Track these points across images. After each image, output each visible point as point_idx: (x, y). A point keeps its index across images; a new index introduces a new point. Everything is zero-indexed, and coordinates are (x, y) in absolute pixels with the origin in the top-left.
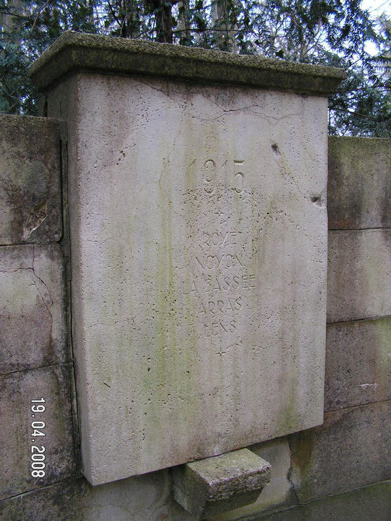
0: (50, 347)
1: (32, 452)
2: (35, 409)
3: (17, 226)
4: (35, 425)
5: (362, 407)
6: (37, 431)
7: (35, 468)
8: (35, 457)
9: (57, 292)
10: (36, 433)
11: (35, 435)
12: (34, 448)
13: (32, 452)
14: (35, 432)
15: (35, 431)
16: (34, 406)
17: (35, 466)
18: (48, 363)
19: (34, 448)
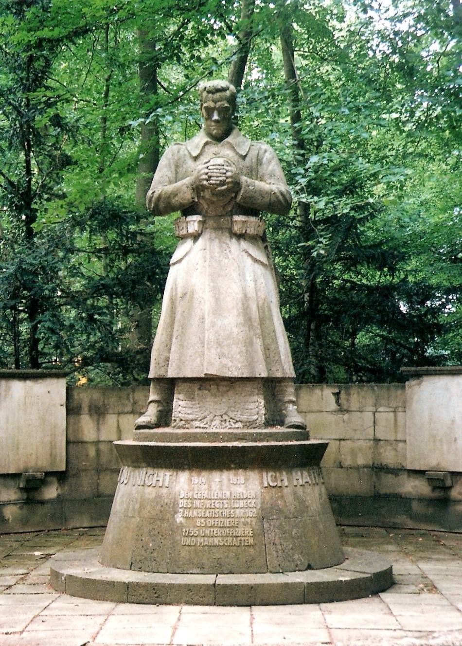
5: (83, 471)
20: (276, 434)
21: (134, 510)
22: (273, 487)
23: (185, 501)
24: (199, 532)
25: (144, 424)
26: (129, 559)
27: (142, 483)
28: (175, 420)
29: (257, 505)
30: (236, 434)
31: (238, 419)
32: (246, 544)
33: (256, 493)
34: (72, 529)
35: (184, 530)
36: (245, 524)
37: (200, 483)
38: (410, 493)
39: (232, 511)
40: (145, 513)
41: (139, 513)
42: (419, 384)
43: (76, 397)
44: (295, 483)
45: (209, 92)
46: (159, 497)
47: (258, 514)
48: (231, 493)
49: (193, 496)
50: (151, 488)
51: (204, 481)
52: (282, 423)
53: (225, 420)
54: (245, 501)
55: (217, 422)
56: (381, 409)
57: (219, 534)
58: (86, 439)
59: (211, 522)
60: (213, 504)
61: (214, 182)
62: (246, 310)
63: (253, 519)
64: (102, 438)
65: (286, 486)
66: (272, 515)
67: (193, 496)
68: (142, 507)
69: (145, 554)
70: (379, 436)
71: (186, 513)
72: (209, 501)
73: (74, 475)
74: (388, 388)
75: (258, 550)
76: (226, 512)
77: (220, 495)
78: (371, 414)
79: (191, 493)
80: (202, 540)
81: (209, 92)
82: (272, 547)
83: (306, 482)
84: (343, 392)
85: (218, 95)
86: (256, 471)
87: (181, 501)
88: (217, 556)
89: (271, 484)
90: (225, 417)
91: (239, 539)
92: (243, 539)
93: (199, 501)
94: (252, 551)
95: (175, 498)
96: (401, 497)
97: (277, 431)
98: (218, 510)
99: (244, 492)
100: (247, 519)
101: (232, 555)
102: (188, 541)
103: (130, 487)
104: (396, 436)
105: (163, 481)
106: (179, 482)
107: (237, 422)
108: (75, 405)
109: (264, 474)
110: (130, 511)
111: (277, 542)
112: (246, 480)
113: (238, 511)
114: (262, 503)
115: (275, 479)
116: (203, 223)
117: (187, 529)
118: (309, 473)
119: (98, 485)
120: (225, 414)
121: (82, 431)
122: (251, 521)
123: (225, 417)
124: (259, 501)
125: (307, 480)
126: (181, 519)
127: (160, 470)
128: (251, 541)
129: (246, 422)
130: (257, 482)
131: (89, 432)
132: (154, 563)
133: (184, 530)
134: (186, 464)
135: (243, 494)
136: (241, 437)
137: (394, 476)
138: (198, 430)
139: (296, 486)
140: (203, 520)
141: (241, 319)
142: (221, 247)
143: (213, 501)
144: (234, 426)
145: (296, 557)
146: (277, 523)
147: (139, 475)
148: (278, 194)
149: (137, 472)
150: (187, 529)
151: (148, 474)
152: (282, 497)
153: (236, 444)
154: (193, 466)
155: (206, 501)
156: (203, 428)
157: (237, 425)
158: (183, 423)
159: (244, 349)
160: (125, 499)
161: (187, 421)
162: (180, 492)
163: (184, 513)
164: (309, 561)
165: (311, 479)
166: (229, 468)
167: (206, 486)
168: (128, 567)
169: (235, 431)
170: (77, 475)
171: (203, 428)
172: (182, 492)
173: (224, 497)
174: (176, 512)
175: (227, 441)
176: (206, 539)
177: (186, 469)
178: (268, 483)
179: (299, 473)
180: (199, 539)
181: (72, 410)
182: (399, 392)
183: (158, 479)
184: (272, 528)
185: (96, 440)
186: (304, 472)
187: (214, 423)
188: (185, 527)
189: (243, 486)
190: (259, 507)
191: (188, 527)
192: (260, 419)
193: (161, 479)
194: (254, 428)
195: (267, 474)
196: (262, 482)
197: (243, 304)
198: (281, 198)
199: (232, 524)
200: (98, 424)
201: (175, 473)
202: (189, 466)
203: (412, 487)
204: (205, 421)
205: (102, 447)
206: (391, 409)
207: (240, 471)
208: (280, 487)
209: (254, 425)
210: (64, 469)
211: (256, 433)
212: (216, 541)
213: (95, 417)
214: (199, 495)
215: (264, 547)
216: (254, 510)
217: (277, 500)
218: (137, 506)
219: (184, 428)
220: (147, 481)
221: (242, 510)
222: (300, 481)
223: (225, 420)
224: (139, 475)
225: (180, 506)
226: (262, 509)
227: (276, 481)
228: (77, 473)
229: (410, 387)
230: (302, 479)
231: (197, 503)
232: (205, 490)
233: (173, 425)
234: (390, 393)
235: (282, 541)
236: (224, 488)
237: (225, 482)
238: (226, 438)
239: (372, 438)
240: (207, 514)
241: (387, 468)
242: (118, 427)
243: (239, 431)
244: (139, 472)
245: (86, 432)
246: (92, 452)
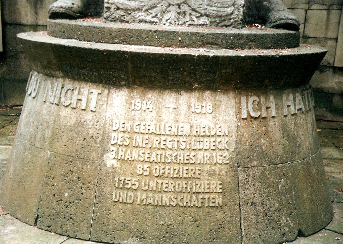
20: (262, 37)
21: (43, 138)
22: (256, 119)
23: (121, 135)
24: (140, 183)
25: (62, 10)
26: (34, 210)
27: (56, 101)
28: (109, 8)
29: (229, 145)
30: (202, 35)
31: (203, 12)
32: (211, 205)
33: (229, 127)
34: (12, 106)
35: (117, 179)
36: (211, 174)
38: (333, 88)
39: (193, 154)
40: (59, 146)
41: (51, 143)
44: (286, 111)
46: (79, 124)
47: (231, 159)
48: (191, 127)
49: (132, 128)
50: (68, 110)
52: (264, 21)
53: (184, 13)
54: (213, 139)
55: (172, 14)
57: (171, 187)
59: (158, 169)
60: (163, 143)
63: (223, 167)
65: (274, 117)
66: (251, 161)
67: (132, 128)
68: (55, 137)
69: (57, 207)
71: (121, 153)
72: (157, 138)
75: (228, 213)
76: (183, 156)
77: (174, 130)
78: (303, 12)
79: (130, 123)
80: (144, 197)
82: (249, 208)
83: (298, 110)
86: (231, 95)
87: (113, 134)
88: (167, 221)
89: (253, 114)
90: (184, 8)
91: (201, 196)
92: (207, 196)
93: (141, 136)
94: (219, 215)
96: (322, 92)
97: (259, 32)
98: (169, 152)
99: (212, 126)
100: (214, 168)
101: (188, 219)
102: (123, 196)
103: (38, 104)
104: (326, 34)
105: (88, 101)
107: (201, 16)
109: (243, 99)
110: (38, 138)
111: (257, 200)
112: (216, 107)
113: (200, 154)
114: (238, 142)
115: (259, 106)
117: (122, 178)
118: (302, 95)
121: (20, 13)
122: (221, 170)
123: (184, 8)
124: (233, 139)
125: (300, 107)
126: (114, 162)
127: (83, 84)
128: (219, 200)
129: (217, 17)
130: (232, 112)
131: (27, 16)
132: (69, 224)
133: (117, 179)
134: (123, 79)
136: (210, 40)
138: (143, 26)
139: (286, 116)
140: (146, 166)
143: (163, 138)
144: (197, 22)
145: (283, 221)
146: (259, 173)
147: (52, 88)
149: (49, 82)
150: (122, 178)
151: (65, 89)
152: (267, 132)
153: (202, 51)
154: (134, 84)
155: (153, 137)
156: (150, 22)
157: (201, 21)
158: (121, 12)
160: (31, 120)
161: (126, 10)
162: (112, 121)
163: (117, 153)
164: (300, 225)
165: (305, 104)
166: (190, 89)
167: (154, 114)
168: (32, 220)
169: (201, 30)
170: (16, 56)
171: (150, 22)
172: (116, 121)
173: (180, 133)
174: (105, 151)
175: (188, 46)
176: (150, 195)
177: (122, 86)
178: (248, 113)
179: (291, 96)
180: (139, 193)
183: (80, 97)
184: (251, 179)
185: (34, 24)
186: (297, 94)
187: (166, 16)
188: (119, 174)
189: (210, 116)
190: (232, 149)
191: (124, 174)
192: (236, 13)
193: (84, 98)
194: (227, 26)
195: (247, 100)
196: (239, 111)
199: (191, 174)
200: (36, 7)
201: (106, 91)
202: (129, 82)
203: (336, 83)
204: (154, 11)
206: (325, 7)
207: (207, 93)
208: (265, 118)
209: (226, 23)
211: (235, 36)
212: (166, 199)
214: (142, 127)
215: (237, 208)
216: (226, 154)
217: (260, 138)
218: (48, 134)
219: (122, 21)
220: (63, 99)
221: (207, 154)
222: (292, 108)
223: (184, 13)
224: (52, 88)
225: (113, 142)
226: (237, 152)
227: (260, 109)
228: (15, 54)
231: (139, 139)
233: (105, 15)
235: (264, 199)
236: (181, 118)
237: (183, 109)
238: (187, 42)
240: (153, 158)
243: (207, 31)
244: (52, 83)
245: (23, 14)
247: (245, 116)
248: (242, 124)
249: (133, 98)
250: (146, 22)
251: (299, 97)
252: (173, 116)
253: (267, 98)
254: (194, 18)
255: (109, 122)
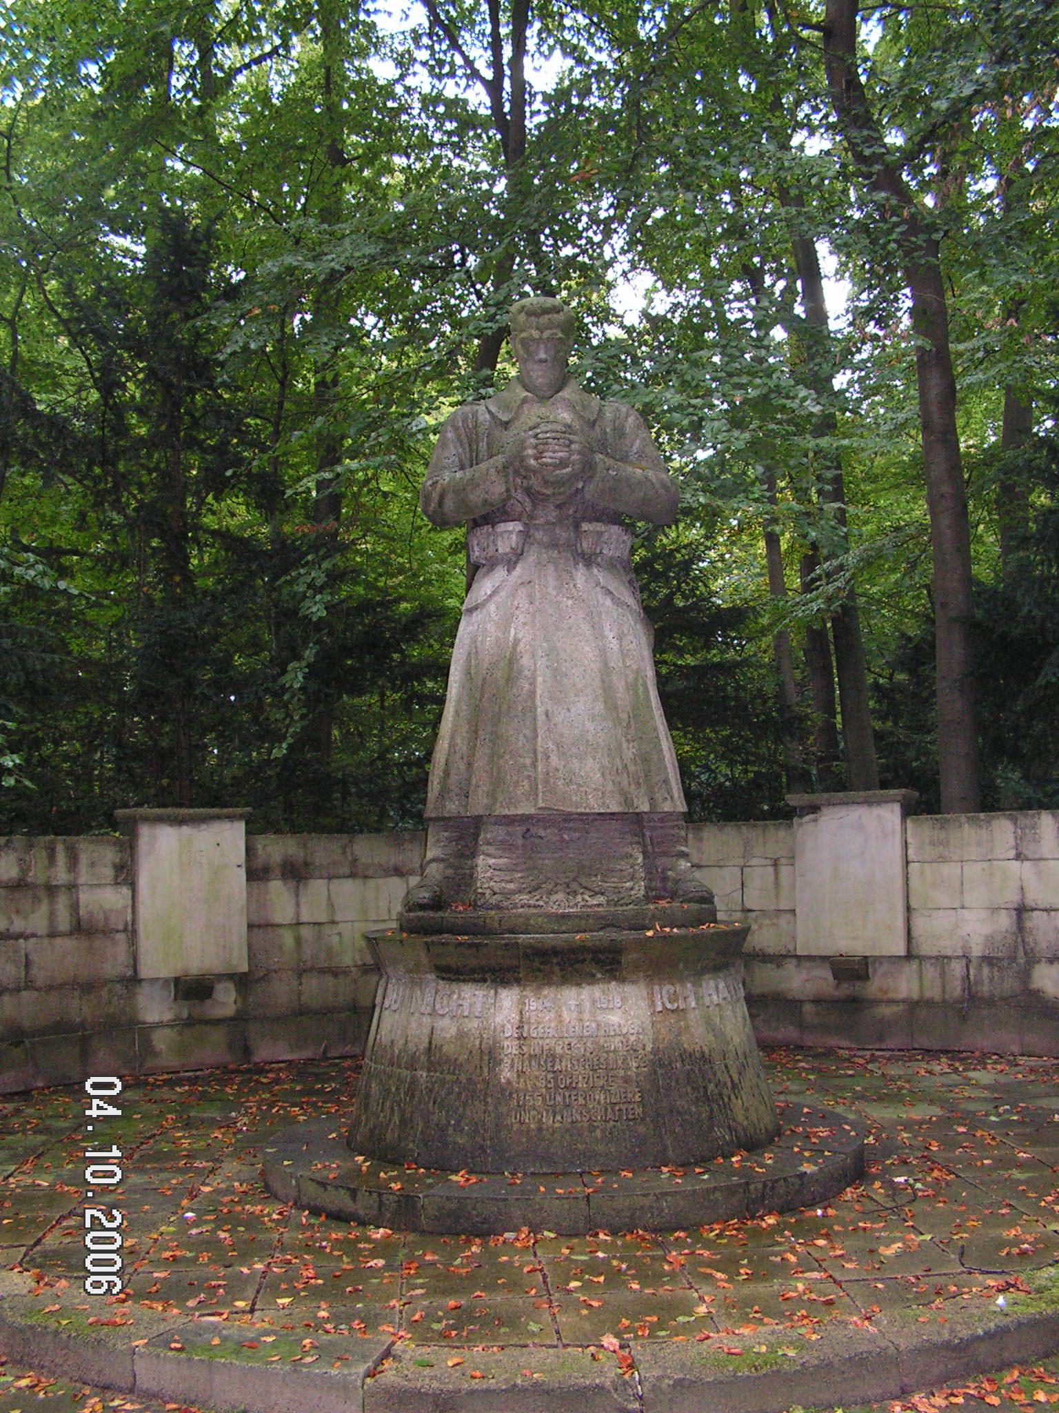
0: (126, 923)
1: (88, 1225)
2: (111, 1284)
3: (116, 877)
4: (95, 1086)
5: (276, 972)
6: (101, 1103)
7: (93, 1269)
8: (95, 1241)
9: (130, 902)
10: (99, 1108)
11: (94, 1113)
12: (92, 1216)
13: (88, 1225)
14: (94, 1106)
15: (95, 1102)
16: (115, 1291)
17: (95, 1263)
18: (125, 930)
19: (92, 1216)
32: (631, 1117)
37: (540, 1008)
42: (815, 820)
43: (260, 852)
45: (529, 314)
51: (547, 1004)
56: (754, 862)
58: (278, 919)
61: (549, 461)
62: (607, 689)
64: (305, 918)
70: (748, 905)
73: (261, 978)
74: (765, 826)
78: (737, 871)
81: (529, 314)
84: (690, 836)
85: (545, 319)
89: (669, 1006)
90: (574, 886)
95: (494, 1037)
106: (501, 1007)
108: (260, 866)
116: (526, 535)
119: (300, 994)
120: (574, 879)
130: (643, 1004)
135: (620, 1026)
137: (774, 966)
141: (600, 707)
142: (559, 578)
148: (658, 486)
156: (535, 906)
159: (606, 761)
162: (503, 1026)
166: (592, 980)
167: (552, 1015)
171: (535, 906)
178: (663, 1004)
181: (256, 873)
182: (782, 833)
196: (653, 1004)
197: (603, 681)
198: (662, 491)
200: (297, 895)
205: (305, 932)
210: (246, 970)
213: (292, 884)
220: (438, 1006)
222: (715, 997)
229: (800, 825)
230: (718, 993)
232: (550, 1021)
234: (773, 839)
236: (586, 1016)
239: (739, 908)
241: (764, 955)
242: (329, 898)
246: (288, 939)
247: (659, 1008)
248: (658, 1018)
249: (526, 997)
250: (529, 906)
251: (722, 985)
252: (575, 1015)
253: (683, 986)
254: (586, 897)
255: (499, 1029)
